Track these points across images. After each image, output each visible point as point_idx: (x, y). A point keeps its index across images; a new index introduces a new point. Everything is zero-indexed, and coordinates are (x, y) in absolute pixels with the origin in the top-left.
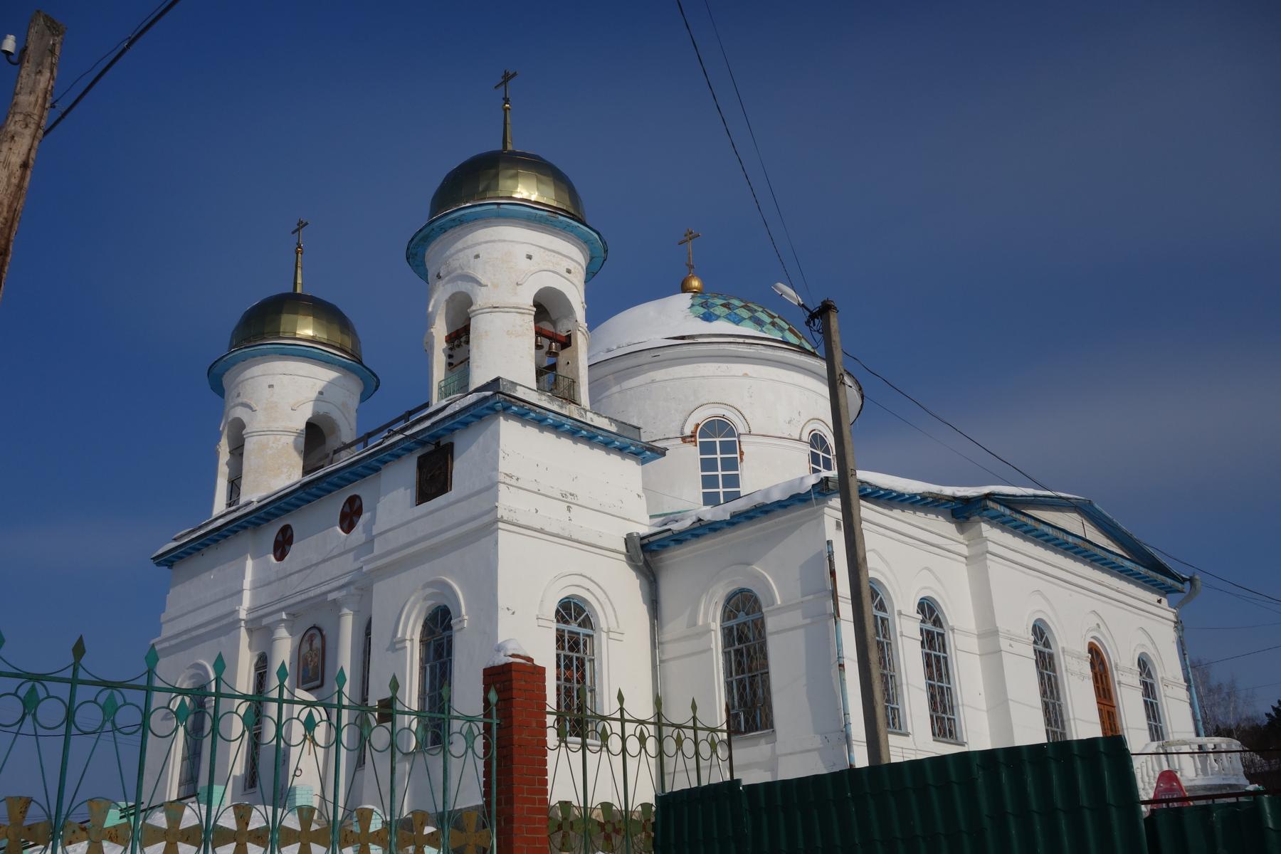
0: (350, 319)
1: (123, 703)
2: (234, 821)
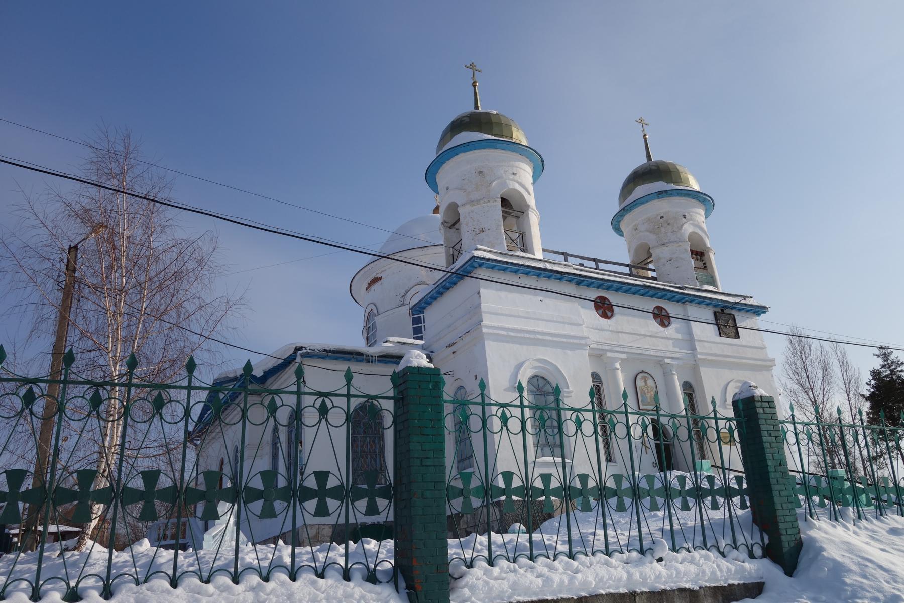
0: (455, 117)
1: (312, 405)
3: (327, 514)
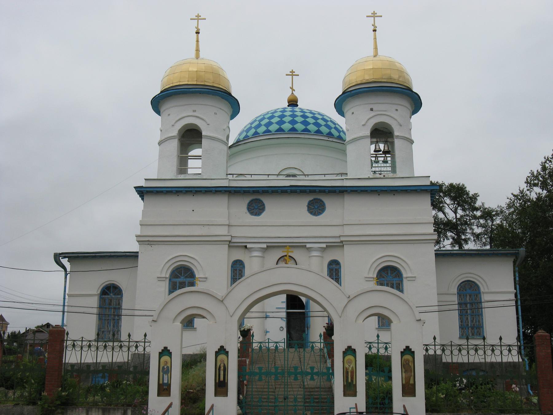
2: (310, 370)
3: (259, 368)
